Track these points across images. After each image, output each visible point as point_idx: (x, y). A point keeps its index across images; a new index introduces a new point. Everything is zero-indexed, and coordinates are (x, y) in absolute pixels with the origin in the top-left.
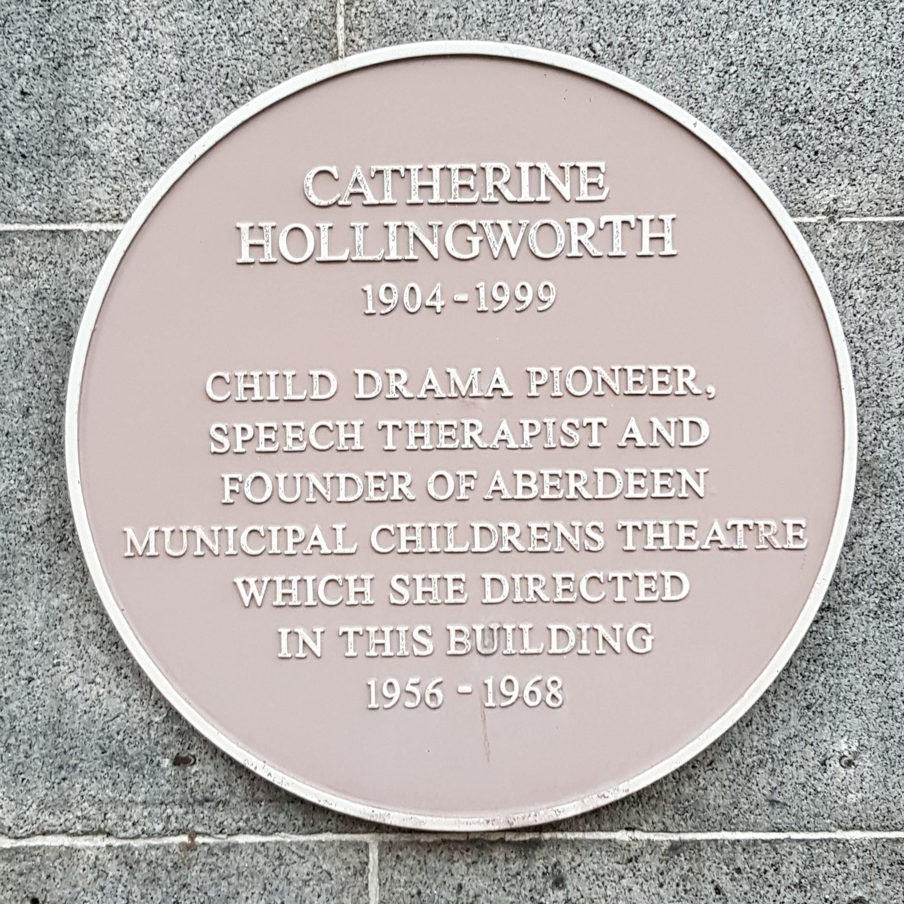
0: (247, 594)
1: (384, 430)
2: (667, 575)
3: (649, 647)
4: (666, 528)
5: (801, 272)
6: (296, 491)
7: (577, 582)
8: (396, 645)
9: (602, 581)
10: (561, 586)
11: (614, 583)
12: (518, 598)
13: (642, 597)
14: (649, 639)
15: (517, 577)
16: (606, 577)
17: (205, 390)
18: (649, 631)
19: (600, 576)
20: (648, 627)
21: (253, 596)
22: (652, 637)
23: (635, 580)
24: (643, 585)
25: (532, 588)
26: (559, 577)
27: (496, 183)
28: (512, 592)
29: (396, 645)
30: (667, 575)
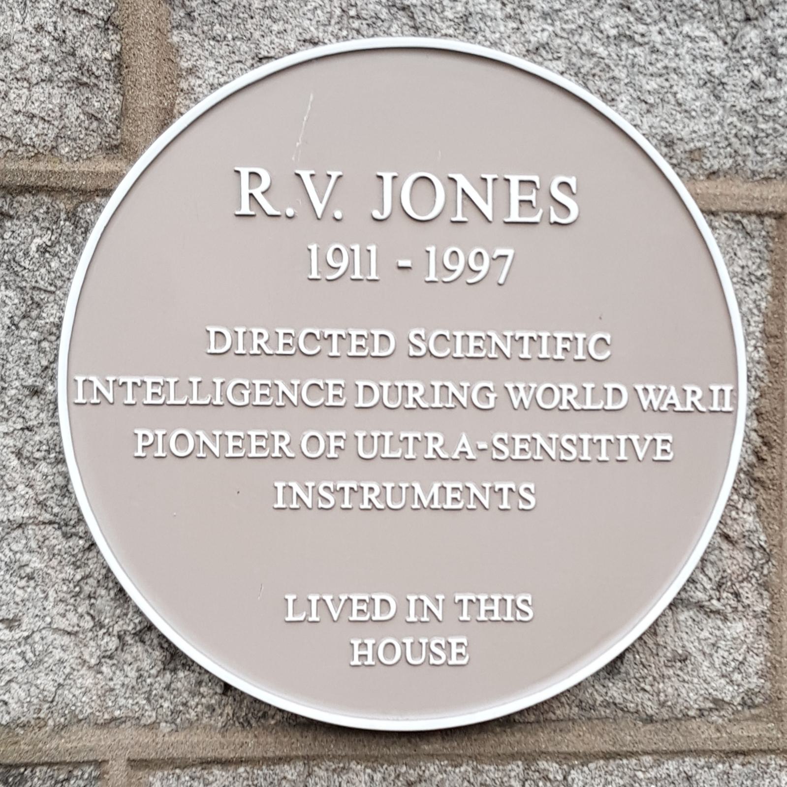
0: (646, 399)
1: (144, 385)
2: (377, 333)
3: (491, 405)
4: (496, 602)
5: (208, 115)
6: (401, 500)
7: (295, 338)
8: (503, 611)
9: (318, 337)
10: (282, 341)
11: (329, 341)
12: (241, 350)
13: (354, 352)
14: (492, 396)
15: (241, 330)
16: (322, 334)
17: (300, 446)
18: (492, 389)
19: (317, 333)
20: (491, 385)
21: (651, 402)
22: (495, 395)
23: (348, 338)
24: (354, 342)
25: (256, 341)
26: (281, 332)
27: (252, 191)
28: (235, 343)
29: (503, 611)
30: (377, 333)
